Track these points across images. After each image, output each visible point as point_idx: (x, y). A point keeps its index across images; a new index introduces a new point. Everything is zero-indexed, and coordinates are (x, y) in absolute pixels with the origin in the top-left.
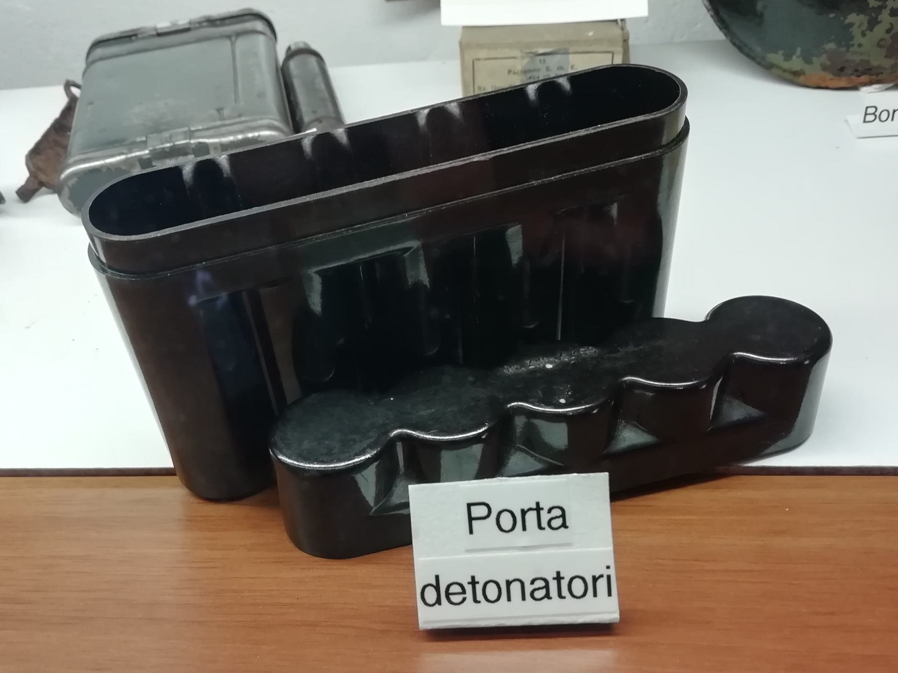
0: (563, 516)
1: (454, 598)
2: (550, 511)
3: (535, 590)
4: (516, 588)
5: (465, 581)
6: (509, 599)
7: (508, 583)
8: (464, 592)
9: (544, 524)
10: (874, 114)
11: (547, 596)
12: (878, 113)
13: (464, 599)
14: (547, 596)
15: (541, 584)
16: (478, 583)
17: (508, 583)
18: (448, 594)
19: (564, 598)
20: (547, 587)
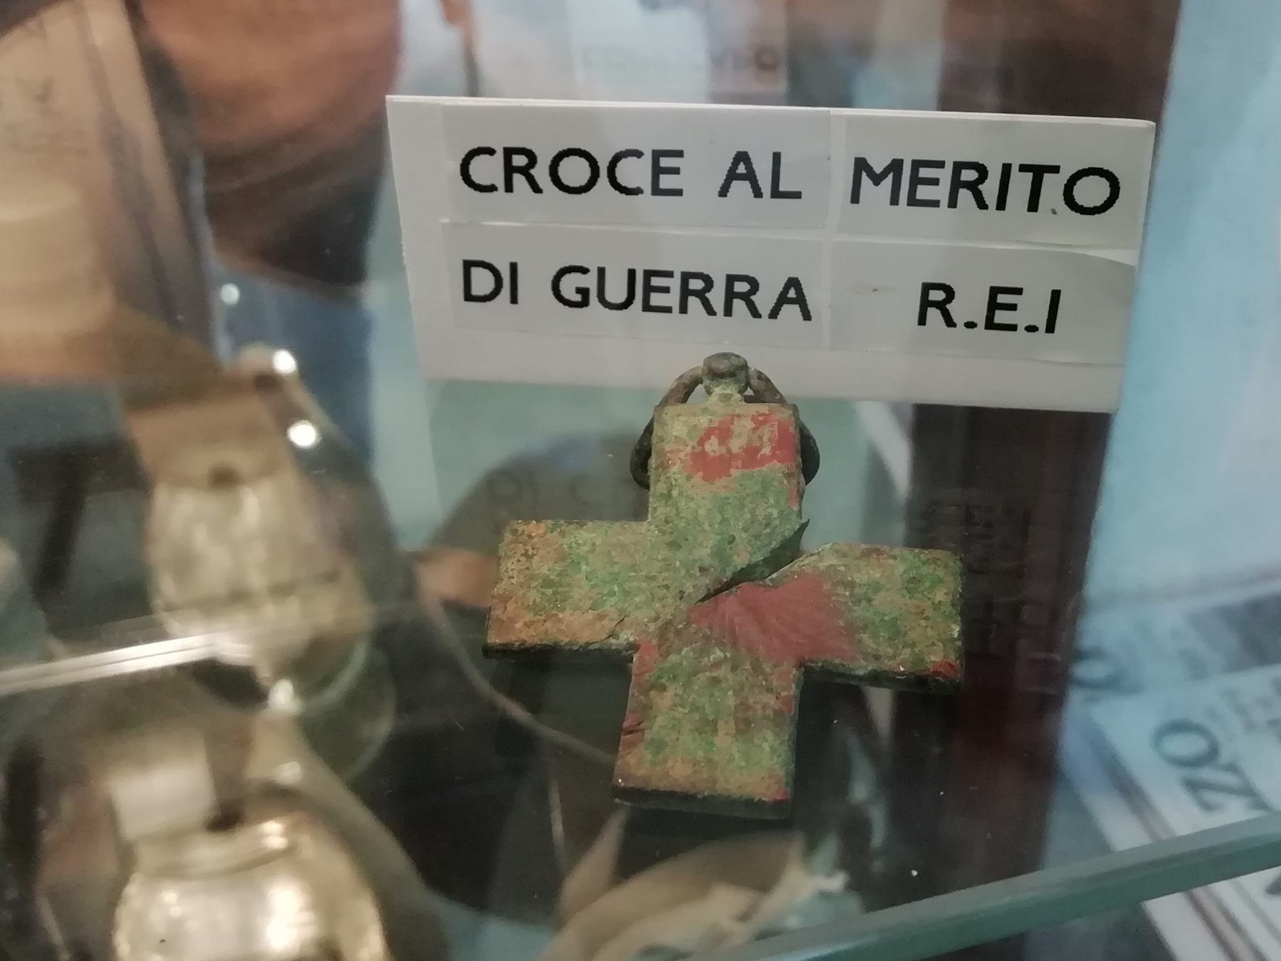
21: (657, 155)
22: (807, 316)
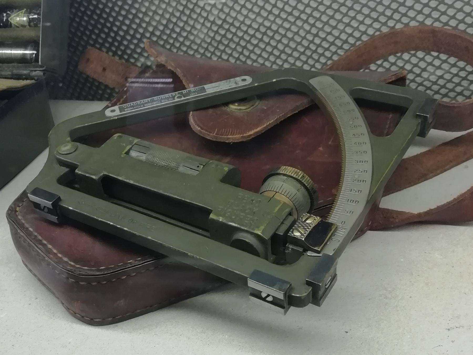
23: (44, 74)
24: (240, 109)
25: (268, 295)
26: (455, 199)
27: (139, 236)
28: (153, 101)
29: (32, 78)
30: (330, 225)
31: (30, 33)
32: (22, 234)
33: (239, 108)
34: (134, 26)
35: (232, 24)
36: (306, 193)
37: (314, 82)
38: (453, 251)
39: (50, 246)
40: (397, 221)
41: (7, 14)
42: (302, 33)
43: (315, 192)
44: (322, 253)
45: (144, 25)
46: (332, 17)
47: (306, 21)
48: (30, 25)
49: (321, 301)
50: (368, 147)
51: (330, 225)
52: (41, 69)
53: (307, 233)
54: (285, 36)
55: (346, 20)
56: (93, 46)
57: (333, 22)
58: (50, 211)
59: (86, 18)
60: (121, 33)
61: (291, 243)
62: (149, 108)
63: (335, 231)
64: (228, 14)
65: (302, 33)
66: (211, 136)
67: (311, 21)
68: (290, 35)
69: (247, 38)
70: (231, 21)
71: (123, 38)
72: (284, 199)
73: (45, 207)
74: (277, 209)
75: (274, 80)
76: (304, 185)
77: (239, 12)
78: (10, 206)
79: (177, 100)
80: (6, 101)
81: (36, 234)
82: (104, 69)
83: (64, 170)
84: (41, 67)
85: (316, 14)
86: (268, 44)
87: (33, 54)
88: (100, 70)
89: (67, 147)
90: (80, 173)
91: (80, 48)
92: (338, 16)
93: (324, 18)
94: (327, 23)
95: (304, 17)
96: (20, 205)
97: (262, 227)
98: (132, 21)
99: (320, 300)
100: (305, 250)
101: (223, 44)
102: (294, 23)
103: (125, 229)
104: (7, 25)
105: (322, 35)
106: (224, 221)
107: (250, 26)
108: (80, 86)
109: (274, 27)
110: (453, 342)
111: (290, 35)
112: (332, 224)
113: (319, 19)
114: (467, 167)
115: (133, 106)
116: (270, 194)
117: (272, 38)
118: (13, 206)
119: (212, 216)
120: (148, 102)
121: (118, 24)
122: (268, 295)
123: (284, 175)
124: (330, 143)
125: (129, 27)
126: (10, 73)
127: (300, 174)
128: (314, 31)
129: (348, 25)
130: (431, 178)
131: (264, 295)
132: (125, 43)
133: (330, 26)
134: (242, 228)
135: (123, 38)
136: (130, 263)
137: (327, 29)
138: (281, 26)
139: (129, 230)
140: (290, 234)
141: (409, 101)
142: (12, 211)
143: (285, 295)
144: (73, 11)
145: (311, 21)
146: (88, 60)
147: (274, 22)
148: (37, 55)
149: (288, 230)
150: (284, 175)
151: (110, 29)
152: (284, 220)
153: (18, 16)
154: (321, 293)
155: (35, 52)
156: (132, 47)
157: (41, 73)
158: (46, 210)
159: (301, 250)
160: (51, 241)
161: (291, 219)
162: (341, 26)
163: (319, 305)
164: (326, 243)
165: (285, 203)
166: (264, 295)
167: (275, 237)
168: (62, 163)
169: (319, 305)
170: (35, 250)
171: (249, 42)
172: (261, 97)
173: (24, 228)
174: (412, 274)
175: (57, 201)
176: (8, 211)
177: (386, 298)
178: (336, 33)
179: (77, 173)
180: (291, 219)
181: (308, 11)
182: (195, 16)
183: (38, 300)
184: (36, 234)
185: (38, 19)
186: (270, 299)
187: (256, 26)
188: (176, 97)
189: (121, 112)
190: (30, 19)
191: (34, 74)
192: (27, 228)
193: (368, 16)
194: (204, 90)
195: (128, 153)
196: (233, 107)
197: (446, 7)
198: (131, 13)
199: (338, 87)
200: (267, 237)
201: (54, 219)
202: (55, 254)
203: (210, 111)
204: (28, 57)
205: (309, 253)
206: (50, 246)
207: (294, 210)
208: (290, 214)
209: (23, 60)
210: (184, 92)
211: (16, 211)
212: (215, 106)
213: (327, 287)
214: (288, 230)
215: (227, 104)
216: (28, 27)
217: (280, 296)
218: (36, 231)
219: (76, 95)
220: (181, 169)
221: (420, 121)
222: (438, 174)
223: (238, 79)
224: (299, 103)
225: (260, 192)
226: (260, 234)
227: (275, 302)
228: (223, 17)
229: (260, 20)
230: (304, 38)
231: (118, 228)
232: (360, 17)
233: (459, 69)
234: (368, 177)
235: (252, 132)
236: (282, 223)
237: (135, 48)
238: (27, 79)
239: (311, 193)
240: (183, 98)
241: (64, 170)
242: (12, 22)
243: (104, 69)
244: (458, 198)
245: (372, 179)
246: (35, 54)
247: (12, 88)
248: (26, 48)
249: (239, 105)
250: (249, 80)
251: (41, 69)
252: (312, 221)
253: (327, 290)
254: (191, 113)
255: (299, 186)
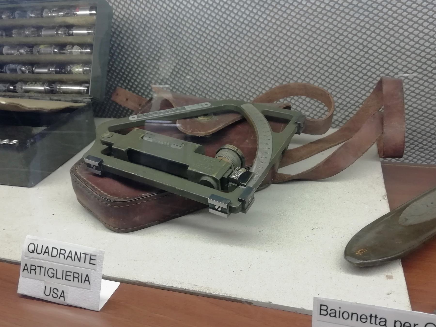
0: (386, 322)
1: (363, 320)
2: (380, 319)
3: (331, 313)
4: (355, 316)
5: (368, 315)
6: (352, 320)
7: (352, 314)
8: (367, 319)
9: (377, 323)
10: (326, 310)
11: (335, 316)
12: (328, 310)
13: (366, 321)
14: (335, 316)
15: (333, 311)
16: (378, 318)
17: (352, 314)
18: (361, 318)
19: (372, 324)
20: (335, 313)
21: (74, 273)
22: (89, 284)
23: (92, 100)
24: (204, 120)
25: (219, 207)
26: (315, 166)
27: (149, 180)
28: (156, 113)
29: (84, 103)
30: (251, 173)
31: (85, 78)
32: (79, 181)
33: (203, 119)
34: (144, 80)
35: (199, 81)
36: (239, 158)
37: (243, 106)
38: (315, 193)
39: (96, 187)
40: (287, 178)
41: (70, 67)
42: (238, 87)
43: (243, 158)
44: (247, 186)
45: (149, 79)
46: (254, 79)
47: (240, 81)
48: (84, 73)
49: (246, 210)
50: (270, 138)
51: (251, 173)
52: (90, 98)
53: (239, 176)
54: (229, 88)
55: (261, 81)
56: (121, 87)
57: (254, 82)
58: (97, 168)
59: (115, 74)
60: (136, 83)
61: (231, 182)
62: (154, 117)
63: (253, 176)
64: (197, 75)
65: (238, 87)
66: (189, 132)
67: (243, 81)
68: (231, 88)
69: (208, 89)
70: (199, 79)
71: (137, 86)
72: (228, 160)
73: (94, 166)
74: (223, 165)
75: (222, 105)
76: (238, 154)
77: (204, 74)
78: (73, 167)
79: (170, 113)
80: (68, 114)
81: (88, 181)
82: (127, 99)
83: (106, 147)
84: (90, 96)
85: (246, 77)
86: (220, 92)
87: (85, 89)
88: (125, 100)
89: (108, 134)
90: (115, 147)
91: (113, 88)
92: (257, 79)
93: (250, 80)
94: (251, 82)
95: (239, 78)
96: (78, 166)
97: (216, 174)
98: (143, 77)
99: (246, 209)
100: (238, 185)
101: (195, 92)
102: (234, 82)
103: (141, 176)
104: (70, 72)
105: (249, 88)
106: (196, 171)
107: (210, 82)
108: (110, 113)
109: (223, 83)
110: (314, 235)
111: (231, 88)
112: (252, 172)
113: (247, 80)
114: (323, 154)
115: (144, 116)
116: (220, 158)
117: (222, 89)
118: (74, 167)
119: (189, 169)
120: (154, 113)
121: (134, 78)
122: (219, 207)
123: (228, 149)
124: (252, 138)
125: (141, 80)
126: (71, 99)
127: (235, 149)
128: (244, 86)
129: (262, 83)
130: (305, 159)
131: (216, 207)
132: (138, 89)
133: (253, 84)
134: (206, 174)
135: (137, 86)
136: (143, 195)
137: (252, 85)
138: (227, 83)
139: (143, 177)
140: (230, 177)
141: (292, 117)
142: (74, 169)
143: (228, 206)
144: (110, 67)
145: (243, 81)
146: (117, 94)
147: (223, 80)
148: (88, 90)
149: (229, 175)
150: (228, 149)
151: (129, 81)
152: (227, 171)
153: (77, 68)
154: (246, 205)
155: (86, 88)
156: (142, 91)
157: (90, 100)
158: (94, 167)
159: (236, 185)
160: (97, 185)
161: (231, 170)
162: (259, 84)
163: (245, 213)
164: (249, 182)
165: (228, 162)
166: (216, 207)
167: (222, 179)
168: (104, 143)
169: (245, 213)
170: (87, 189)
171: (209, 91)
172: (215, 114)
173: (81, 178)
174: (294, 204)
175: (101, 163)
176: (71, 169)
177: (281, 215)
178: (256, 88)
179: (113, 148)
180: (231, 170)
181: (241, 75)
182: (179, 76)
183: (86, 221)
184: (88, 181)
185: (90, 70)
186: (220, 209)
187: (213, 82)
188: (169, 112)
189: (138, 118)
190: (84, 70)
191: (85, 100)
192: (83, 178)
193: (273, 79)
194: (185, 109)
195: (142, 138)
196: (201, 119)
197: (313, 76)
198: (142, 72)
199: (256, 109)
200: (218, 178)
201: (99, 173)
202: (99, 191)
203: (188, 120)
204: (82, 91)
205: (240, 186)
206: (96, 187)
207: (233, 166)
208: (231, 168)
209: (79, 93)
210: (174, 109)
211: (76, 170)
212: (191, 118)
213: (249, 203)
214: (229, 175)
215: (197, 117)
216: (83, 74)
217: (225, 206)
218: (88, 180)
219: (109, 115)
220: (173, 146)
221: (297, 125)
222: (308, 157)
223: (203, 104)
224: (236, 118)
225: (215, 157)
226: (215, 177)
227: (223, 211)
228: (195, 76)
229: (215, 79)
230: (239, 90)
231: (137, 176)
232: (269, 80)
233: (320, 109)
234: (270, 151)
235: (211, 131)
236: (226, 172)
237: (144, 92)
238: (81, 103)
239: (241, 158)
240: (173, 112)
241: (106, 147)
242: (73, 71)
243: (127, 99)
244: (317, 165)
245: (272, 152)
246: (87, 90)
247: (73, 107)
248: (81, 86)
249: (204, 118)
250: (209, 104)
251: (90, 98)
252: (242, 171)
253: (249, 205)
254: (178, 120)
255: (235, 154)
